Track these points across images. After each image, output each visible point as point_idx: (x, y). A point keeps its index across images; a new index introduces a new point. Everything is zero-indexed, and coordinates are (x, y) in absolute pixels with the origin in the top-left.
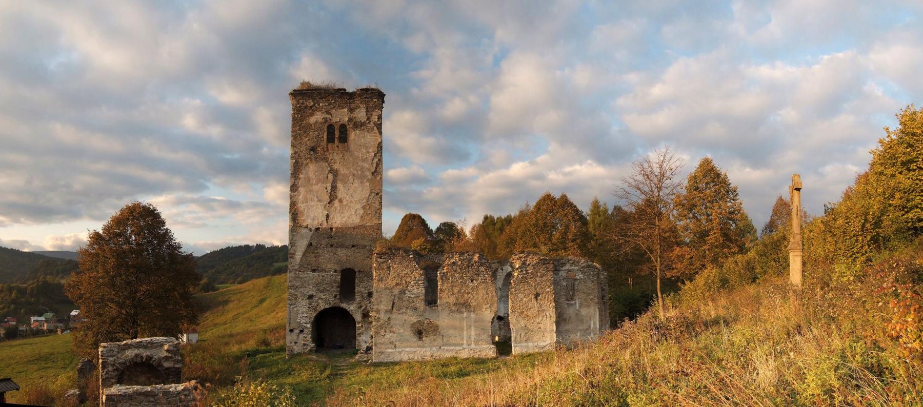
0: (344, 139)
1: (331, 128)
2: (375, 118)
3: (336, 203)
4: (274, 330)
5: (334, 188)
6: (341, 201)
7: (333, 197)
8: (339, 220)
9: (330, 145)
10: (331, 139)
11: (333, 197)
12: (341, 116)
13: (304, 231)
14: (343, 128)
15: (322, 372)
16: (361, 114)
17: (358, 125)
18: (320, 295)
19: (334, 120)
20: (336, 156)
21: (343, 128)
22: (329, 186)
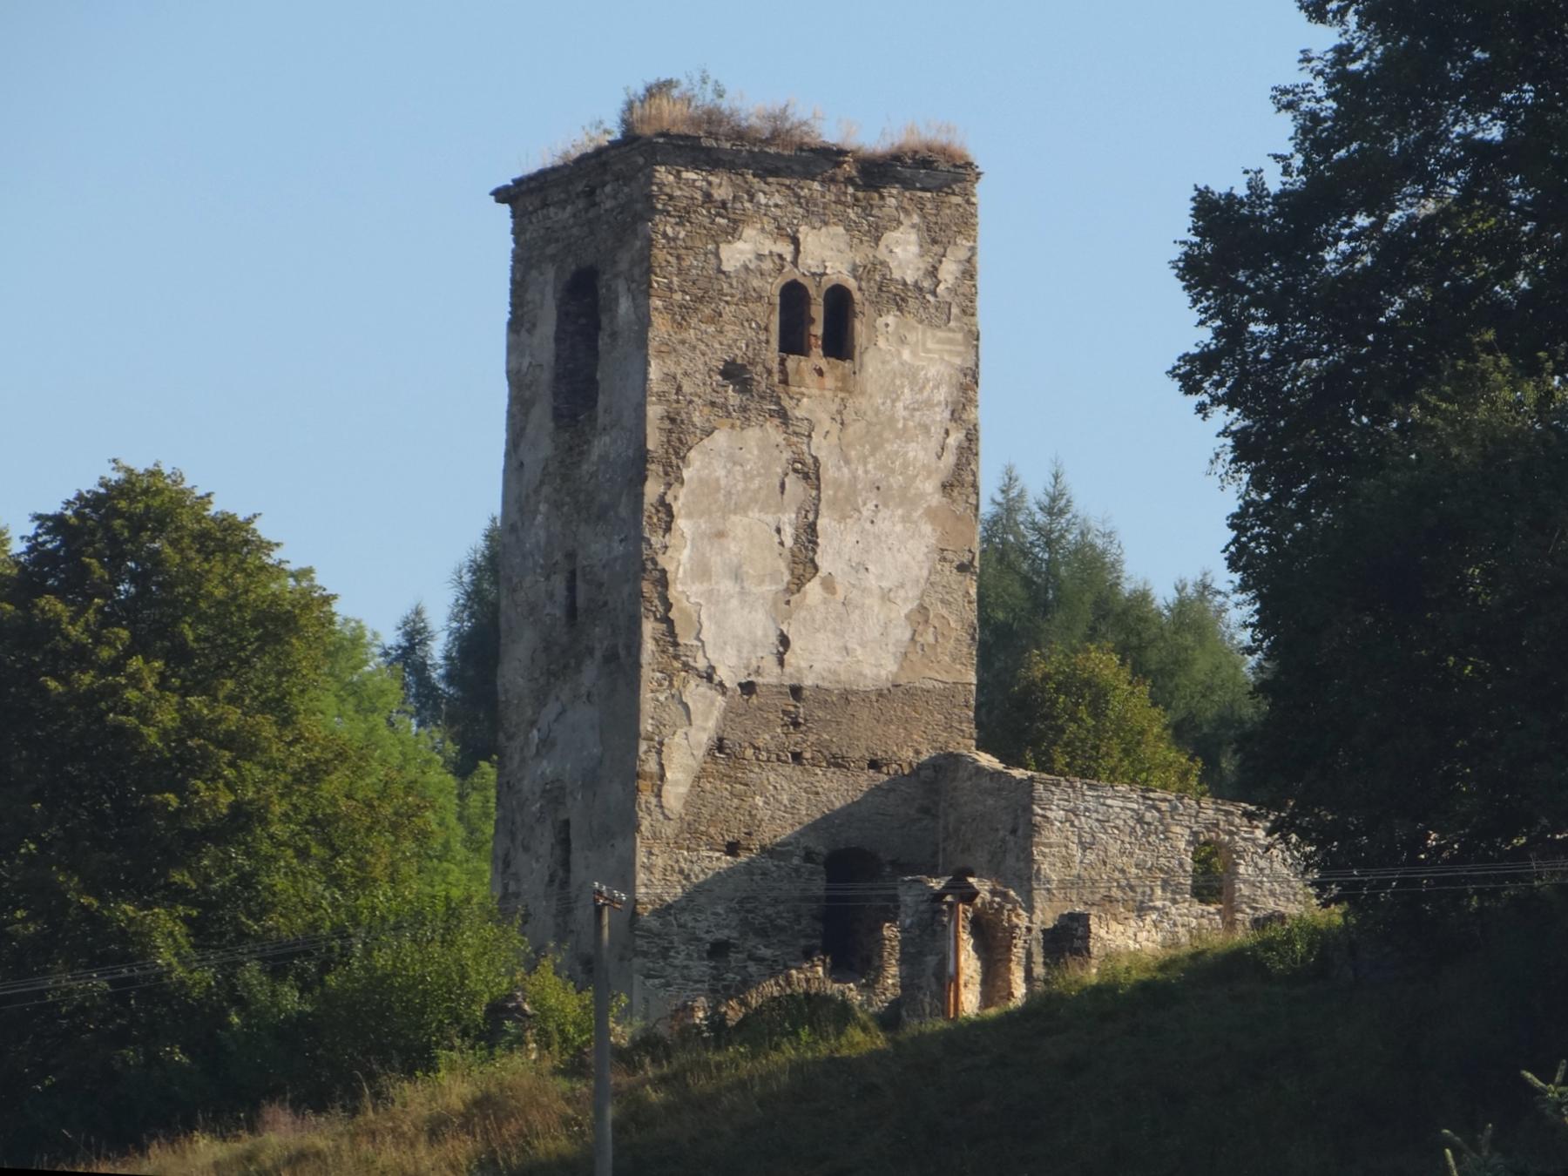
0: (839, 344)
1: (794, 296)
2: (949, 271)
3: (813, 588)
4: (987, 540)
5: (809, 534)
6: (829, 585)
7: (803, 560)
8: (816, 660)
9: (792, 361)
10: (793, 341)
11: (803, 560)
12: (827, 253)
13: (695, 692)
14: (840, 302)
15: (1478, 1152)
16: (904, 251)
17: (897, 297)
18: (752, 942)
19: (809, 261)
20: (813, 389)
21: (840, 302)
22: (788, 520)
